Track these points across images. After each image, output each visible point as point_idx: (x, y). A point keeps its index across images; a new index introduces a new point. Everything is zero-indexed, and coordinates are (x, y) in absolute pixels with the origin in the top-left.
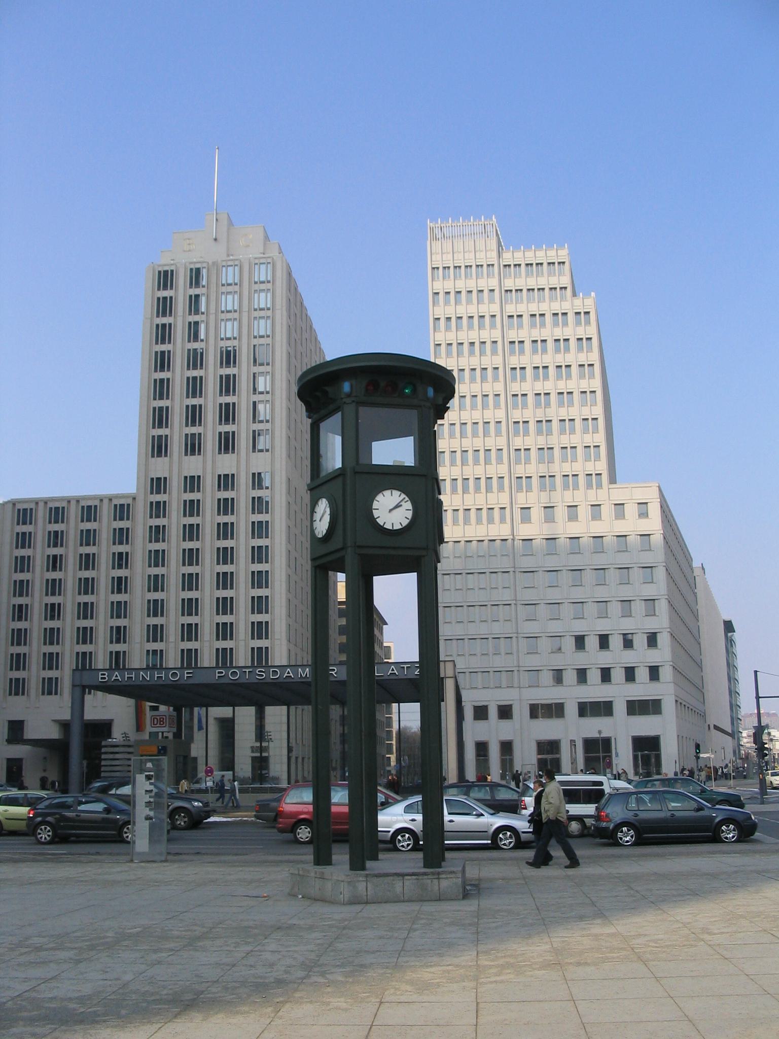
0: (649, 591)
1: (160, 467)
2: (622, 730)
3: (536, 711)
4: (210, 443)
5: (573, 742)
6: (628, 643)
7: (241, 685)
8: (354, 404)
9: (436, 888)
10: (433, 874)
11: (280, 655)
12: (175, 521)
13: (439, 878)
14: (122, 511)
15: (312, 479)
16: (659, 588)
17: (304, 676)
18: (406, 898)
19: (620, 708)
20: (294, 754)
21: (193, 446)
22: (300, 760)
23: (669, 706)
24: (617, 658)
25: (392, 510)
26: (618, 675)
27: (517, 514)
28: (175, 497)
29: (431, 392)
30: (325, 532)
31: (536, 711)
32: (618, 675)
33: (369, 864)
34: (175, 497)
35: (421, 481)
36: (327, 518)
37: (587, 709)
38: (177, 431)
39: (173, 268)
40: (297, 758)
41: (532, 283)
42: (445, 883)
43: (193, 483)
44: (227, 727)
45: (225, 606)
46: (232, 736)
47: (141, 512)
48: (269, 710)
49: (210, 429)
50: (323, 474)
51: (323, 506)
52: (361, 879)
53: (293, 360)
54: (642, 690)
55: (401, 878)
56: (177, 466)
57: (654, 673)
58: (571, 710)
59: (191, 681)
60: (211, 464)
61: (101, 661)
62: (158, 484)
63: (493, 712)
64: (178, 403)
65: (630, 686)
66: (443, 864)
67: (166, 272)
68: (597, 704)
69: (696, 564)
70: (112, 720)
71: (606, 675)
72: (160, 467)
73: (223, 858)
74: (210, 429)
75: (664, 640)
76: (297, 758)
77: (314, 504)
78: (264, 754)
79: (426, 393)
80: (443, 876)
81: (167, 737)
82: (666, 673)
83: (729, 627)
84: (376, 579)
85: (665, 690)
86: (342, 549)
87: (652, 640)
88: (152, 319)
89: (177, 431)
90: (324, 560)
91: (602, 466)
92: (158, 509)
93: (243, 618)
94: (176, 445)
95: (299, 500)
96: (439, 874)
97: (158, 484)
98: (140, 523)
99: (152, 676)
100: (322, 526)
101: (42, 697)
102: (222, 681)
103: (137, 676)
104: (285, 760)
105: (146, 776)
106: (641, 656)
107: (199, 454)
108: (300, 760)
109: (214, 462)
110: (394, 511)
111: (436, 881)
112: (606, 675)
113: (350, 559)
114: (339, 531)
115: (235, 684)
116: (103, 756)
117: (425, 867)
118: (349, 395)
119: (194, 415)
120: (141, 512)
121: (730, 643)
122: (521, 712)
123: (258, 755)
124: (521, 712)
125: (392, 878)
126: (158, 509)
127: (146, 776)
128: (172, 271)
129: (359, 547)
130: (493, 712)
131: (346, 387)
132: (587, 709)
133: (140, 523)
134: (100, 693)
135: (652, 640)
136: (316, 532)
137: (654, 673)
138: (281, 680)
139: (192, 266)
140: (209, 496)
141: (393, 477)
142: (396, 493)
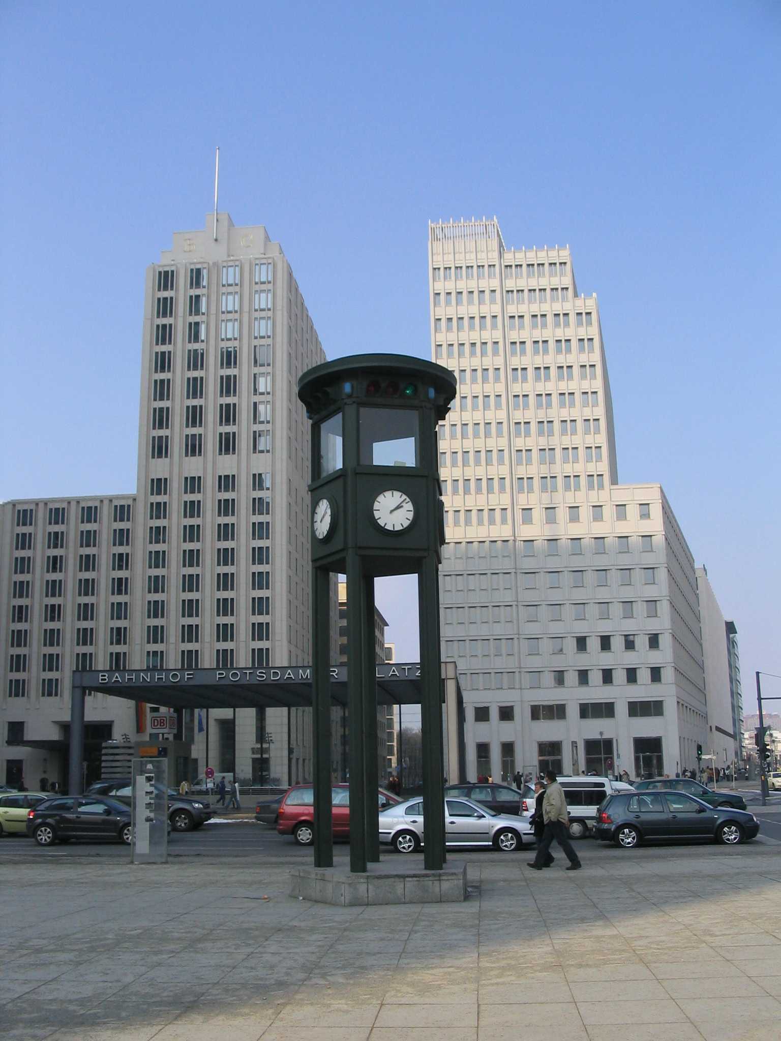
0: (651, 592)
1: (160, 468)
2: (623, 731)
3: (537, 712)
4: (211, 444)
6: (630, 644)
7: (242, 687)
8: (355, 406)
9: (437, 889)
11: (280, 657)
12: (175, 522)
14: (123, 512)
15: (313, 479)
16: (661, 589)
19: (621, 710)
20: (294, 756)
21: (194, 447)
22: (301, 761)
23: (670, 707)
24: (618, 659)
25: (393, 511)
26: (620, 676)
27: (519, 515)
28: (176, 498)
29: (432, 393)
30: (326, 533)
31: (537, 712)
32: (620, 676)
33: (370, 865)
34: (176, 498)
35: (422, 483)
36: (328, 519)
37: (588, 711)
38: (178, 432)
39: (173, 268)
40: (297, 759)
41: (533, 283)
43: (193, 484)
44: (228, 729)
45: (226, 532)
47: (141, 513)
48: (270, 712)
49: (211, 430)
50: (324, 475)
51: (324, 507)
52: (362, 880)
54: (644, 691)
55: (402, 880)
56: (178, 466)
57: (656, 674)
58: (573, 711)
59: (191, 683)
60: (211, 465)
61: (102, 662)
62: (159, 485)
63: (494, 714)
64: (178, 403)
66: (444, 865)
67: (166, 273)
69: (698, 565)
70: (113, 721)
71: (607, 677)
72: (160, 468)
73: (223, 860)
74: (211, 430)
75: (665, 641)
76: (297, 759)
77: (315, 505)
78: (265, 756)
79: (427, 393)
81: (167, 739)
84: (377, 580)
85: (667, 692)
87: (654, 641)
88: (152, 320)
89: (178, 432)
90: (325, 561)
91: (603, 467)
92: (159, 510)
94: (177, 447)
95: (299, 500)
96: (440, 875)
97: (159, 485)
98: (141, 524)
99: (152, 678)
100: (323, 527)
101: (42, 699)
102: (223, 682)
103: (137, 677)
105: (147, 777)
106: (643, 658)
108: (301, 761)
109: (214, 463)
110: (395, 512)
112: (607, 677)
113: (351, 558)
114: (340, 533)
115: (235, 686)
116: (103, 758)
117: (426, 868)
120: (141, 513)
122: (522, 713)
123: (259, 756)
124: (522, 713)
125: (393, 880)
126: (159, 510)
127: (147, 777)
128: (172, 272)
130: (494, 714)
131: (347, 387)
132: (588, 711)
133: (141, 524)
134: (100, 695)
135: (654, 641)
136: (317, 533)
137: (656, 674)
138: (282, 681)
139: (193, 267)
140: (210, 496)
141: (394, 478)
142: (397, 494)
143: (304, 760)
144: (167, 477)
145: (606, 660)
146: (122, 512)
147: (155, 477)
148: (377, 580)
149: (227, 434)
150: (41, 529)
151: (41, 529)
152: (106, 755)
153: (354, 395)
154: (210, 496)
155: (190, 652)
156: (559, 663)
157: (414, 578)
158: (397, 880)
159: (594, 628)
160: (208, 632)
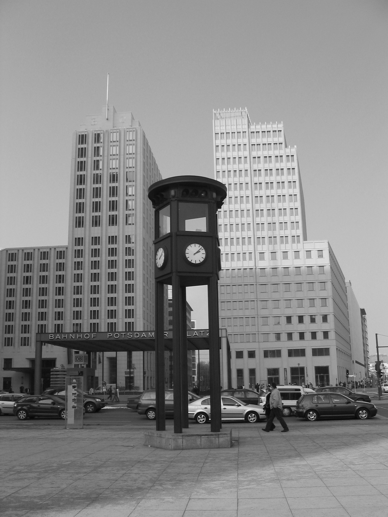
1: (79, 232)
2: (310, 363)
3: (267, 354)
4: (105, 221)
5: (285, 369)
6: (313, 320)
8: (176, 201)
9: (217, 442)
10: (216, 435)
11: (139, 326)
12: (87, 259)
13: (218, 437)
14: (61, 254)
15: (156, 238)
17: (151, 336)
18: (202, 447)
19: (309, 352)
20: (146, 375)
21: (96, 222)
22: (149, 378)
23: (333, 351)
24: (307, 327)
25: (195, 254)
26: (308, 336)
28: (87, 247)
29: (214, 195)
31: (267, 354)
32: (308, 336)
33: (184, 430)
34: (87, 247)
35: (210, 240)
36: (163, 258)
37: (292, 353)
38: (88, 214)
39: (86, 133)
40: (148, 377)
42: (221, 440)
43: (96, 240)
44: (113, 362)
46: (116, 366)
47: (70, 255)
48: (134, 353)
49: (105, 213)
50: (161, 236)
51: (161, 252)
52: (180, 437)
53: (146, 179)
54: (320, 343)
56: (88, 232)
57: (326, 335)
59: (95, 339)
60: (105, 231)
61: (50, 329)
62: (79, 241)
63: (246, 354)
64: (89, 200)
65: (314, 342)
66: (221, 430)
67: (83, 135)
68: (298, 350)
69: (347, 281)
70: (56, 358)
71: (302, 336)
72: (79, 232)
73: (111, 427)
74: (105, 213)
75: (331, 318)
76: (148, 377)
77: (156, 251)
78: (132, 375)
79: (212, 195)
80: (221, 436)
81: (83, 367)
82: (332, 335)
83: (363, 312)
84: (187, 288)
85: (331, 344)
86: (170, 273)
87: (325, 318)
88: (76, 159)
89: (88, 214)
92: (79, 253)
93: (121, 307)
94: (88, 222)
95: (149, 249)
96: (219, 435)
97: (79, 241)
98: (70, 260)
99: (76, 336)
100: (160, 262)
101: (21, 347)
102: (111, 339)
103: (68, 336)
104: (142, 378)
105: (73, 386)
106: (319, 327)
107: (99, 226)
108: (149, 378)
110: (197, 254)
111: (217, 439)
112: (302, 336)
115: (117, 341)
116: (51, 376)
118: (174, 197)
119: (97, 207)
120: (70, 255)
121: (363, 320)
122: (259, 354)
123: (128, 375)
124: (259, 354)
125: (195, 437)
126: (79, 253)
127: (73, 386)
128: (86, 135)
129: (179, 272)
130: (246, 354)
131: (173, 192)
132: (292, 353)
133: (70, 260)
134: (50, 345)
135: (325, 318)
136: (158, 265)
137: (326, 335)
138: (140, 338)
139: (96, 132)
140: (104, 247)
141: (196, 237)
142: (197, 245)
143: (151, 377)
144: (83, 236)
145: (301, 328)
146: (61, 254)
147: (77, 237)
148: (187, 288)
149: (113, 215)
150: (20, 263)
151: (20, 263)
152: (53, 375)
153: (176, 196)
154: (104, 247)
155: (94, 324)
156: (278, 329)
157: (205, 287)
158: (197, 437)
159: (295, 312)
160: (103, 314)
